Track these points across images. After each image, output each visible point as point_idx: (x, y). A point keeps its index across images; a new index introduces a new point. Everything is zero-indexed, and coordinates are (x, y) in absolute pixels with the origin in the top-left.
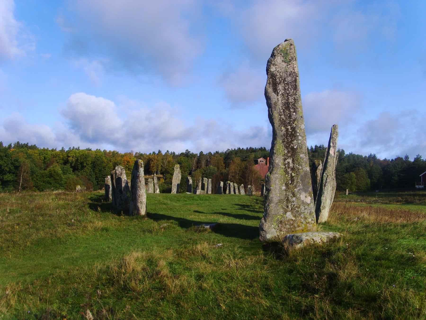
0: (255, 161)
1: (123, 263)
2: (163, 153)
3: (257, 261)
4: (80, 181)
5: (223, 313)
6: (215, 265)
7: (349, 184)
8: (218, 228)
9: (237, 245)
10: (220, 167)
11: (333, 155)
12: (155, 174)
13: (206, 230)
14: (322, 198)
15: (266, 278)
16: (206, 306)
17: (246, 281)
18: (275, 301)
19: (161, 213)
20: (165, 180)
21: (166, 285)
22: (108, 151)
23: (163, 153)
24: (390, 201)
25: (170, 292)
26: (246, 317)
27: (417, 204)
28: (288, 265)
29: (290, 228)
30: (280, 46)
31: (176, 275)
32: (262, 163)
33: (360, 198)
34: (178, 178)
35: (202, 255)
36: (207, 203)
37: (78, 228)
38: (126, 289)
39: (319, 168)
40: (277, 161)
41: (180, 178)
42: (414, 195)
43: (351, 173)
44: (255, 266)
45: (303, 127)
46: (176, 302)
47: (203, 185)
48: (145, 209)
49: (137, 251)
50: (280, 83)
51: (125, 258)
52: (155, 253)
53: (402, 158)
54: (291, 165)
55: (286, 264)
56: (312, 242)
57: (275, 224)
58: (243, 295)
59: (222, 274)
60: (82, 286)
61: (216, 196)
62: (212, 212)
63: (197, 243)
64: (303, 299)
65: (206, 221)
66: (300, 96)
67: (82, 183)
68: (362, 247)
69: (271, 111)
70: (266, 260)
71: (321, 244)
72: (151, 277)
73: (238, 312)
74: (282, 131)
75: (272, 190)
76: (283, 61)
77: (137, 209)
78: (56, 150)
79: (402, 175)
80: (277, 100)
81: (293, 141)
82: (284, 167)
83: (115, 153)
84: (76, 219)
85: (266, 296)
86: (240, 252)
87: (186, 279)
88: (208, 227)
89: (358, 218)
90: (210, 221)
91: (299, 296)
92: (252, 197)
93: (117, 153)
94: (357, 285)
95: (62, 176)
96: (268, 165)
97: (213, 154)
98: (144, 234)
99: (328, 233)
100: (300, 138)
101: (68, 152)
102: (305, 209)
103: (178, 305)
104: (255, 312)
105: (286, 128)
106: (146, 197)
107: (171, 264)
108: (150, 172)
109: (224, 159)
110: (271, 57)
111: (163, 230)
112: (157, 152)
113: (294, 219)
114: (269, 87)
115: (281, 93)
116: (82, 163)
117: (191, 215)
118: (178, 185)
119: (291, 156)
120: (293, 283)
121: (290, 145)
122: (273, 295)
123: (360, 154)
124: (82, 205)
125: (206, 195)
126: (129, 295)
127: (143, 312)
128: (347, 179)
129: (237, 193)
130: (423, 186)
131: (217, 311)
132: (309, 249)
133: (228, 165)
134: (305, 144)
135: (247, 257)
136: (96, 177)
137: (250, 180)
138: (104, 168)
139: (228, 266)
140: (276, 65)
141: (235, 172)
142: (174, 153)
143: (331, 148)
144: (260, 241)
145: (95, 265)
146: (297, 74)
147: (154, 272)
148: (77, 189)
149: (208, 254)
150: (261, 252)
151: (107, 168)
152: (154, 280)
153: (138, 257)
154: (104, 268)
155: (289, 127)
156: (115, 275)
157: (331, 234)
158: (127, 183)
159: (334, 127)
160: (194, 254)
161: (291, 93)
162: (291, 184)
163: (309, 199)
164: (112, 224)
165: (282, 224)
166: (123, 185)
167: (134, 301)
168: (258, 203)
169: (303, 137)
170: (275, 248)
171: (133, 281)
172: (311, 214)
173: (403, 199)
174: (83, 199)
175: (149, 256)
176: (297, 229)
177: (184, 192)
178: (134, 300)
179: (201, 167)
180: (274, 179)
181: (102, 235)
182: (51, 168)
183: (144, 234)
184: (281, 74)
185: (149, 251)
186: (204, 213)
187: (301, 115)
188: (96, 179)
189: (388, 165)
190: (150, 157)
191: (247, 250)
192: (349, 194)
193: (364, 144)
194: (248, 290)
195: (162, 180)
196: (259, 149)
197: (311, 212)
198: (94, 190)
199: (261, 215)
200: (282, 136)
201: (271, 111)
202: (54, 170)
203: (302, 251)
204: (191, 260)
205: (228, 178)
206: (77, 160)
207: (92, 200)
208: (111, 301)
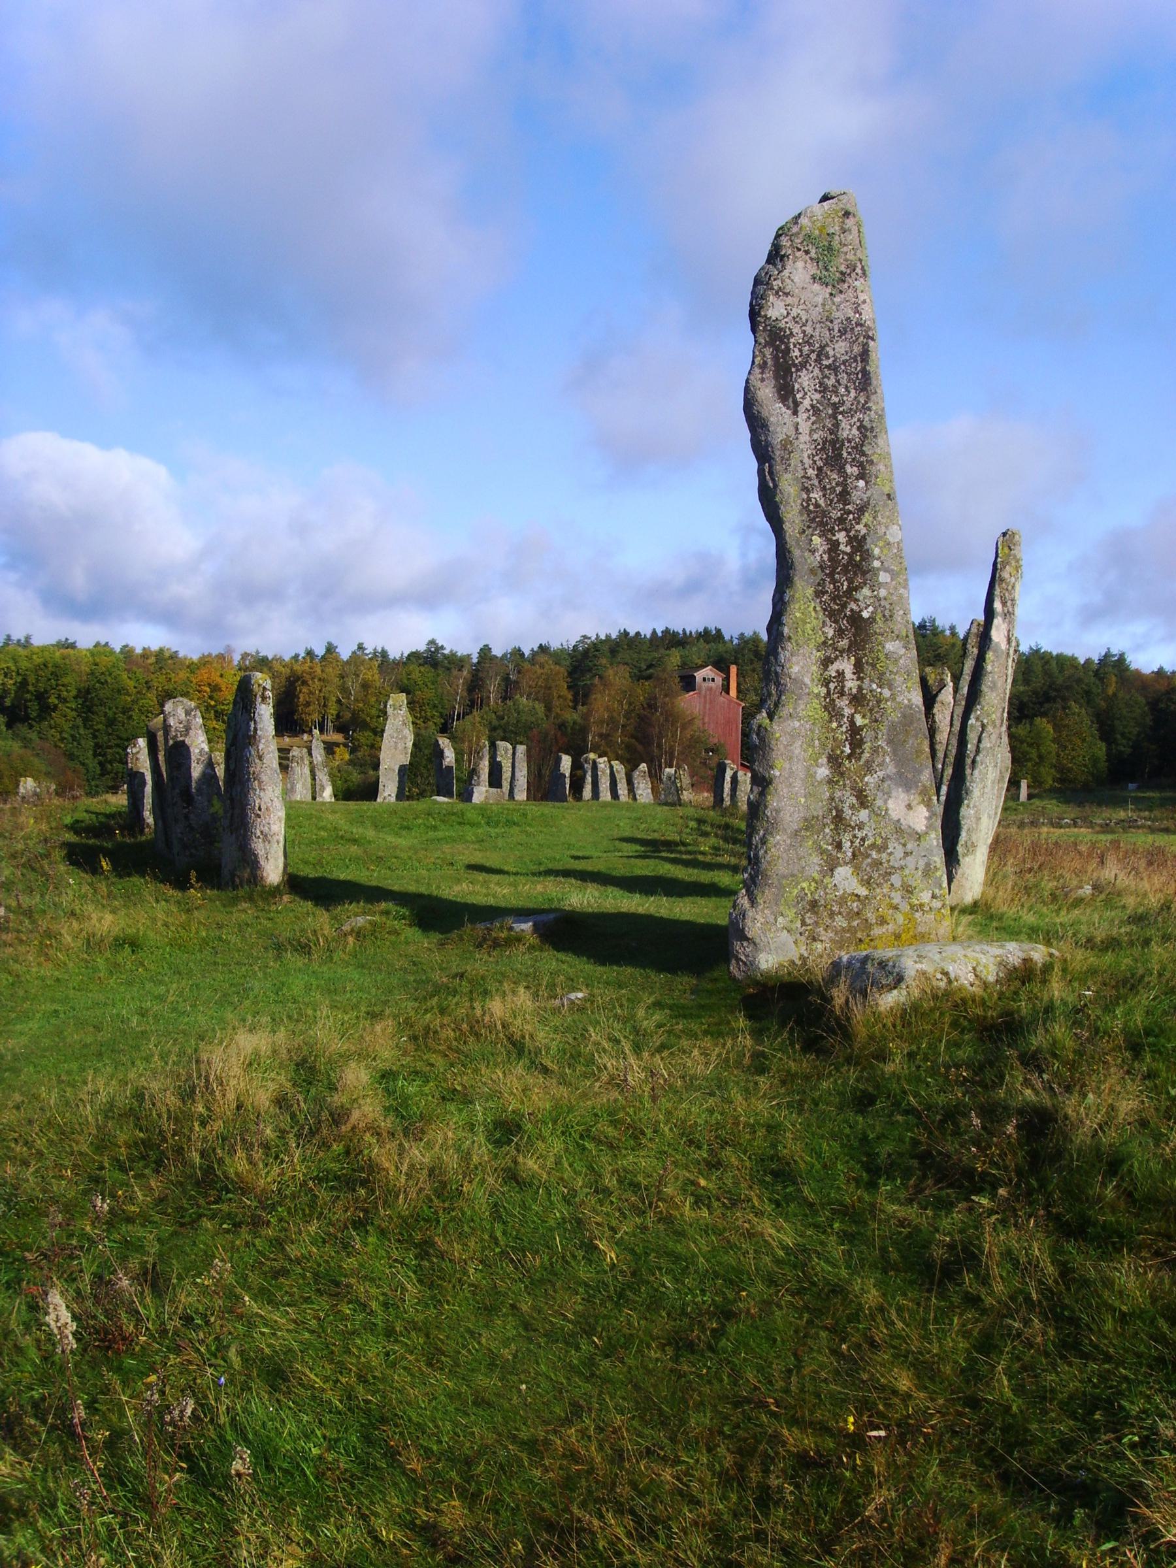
0: (682, 678)
1: (199, 1078)
2: (345, 653)
3: (727, 1060)
4: (36, 761)
5: (608, 1278)
6: (563, 1081)
7: (1030, 759)
8: (565, 932)
9: (643, 996)
10: (556, 702)
11: (1004, 646)
12: (316, 732)
13: (519, 940)
14: (963, 811)
15: (772, 1128)
16: (537, 1252)
17: (691, 1142)
18: (816, 1226)
19: (342, 877)
20: (353, 751)
21: (372, 1167)
22: (139, 651)
23: (345, 653)
25: (392, 1193)
26: (703, 1292)
28: (853, 1074)
29: (850, 929)
30: (804, 221)
31: (410, 1124)
33: (1070, 812)
34: (401, 746)
35: (510, 1038)
36: (510, 838)
37: (21, 941)
38: (210, 1182)
39: (940, 697)
40: (795, 669)
41: (410, 744)
43: (1038, 720)
44: (719, 1080)
45: (894, 534)
46: (418, 1240)
48: (281, 860)
49: (252, 1030)
50: (803, 365)
51: (204, 1057)
52: (326, 1034)
55: (844, 1069)
56: (942, 984)
57: (791, 913)
58: (683, 1203)
59: (596, 1115)
60: (37, 1171)
61: (548, 808)
62: (534, 868)
63: (486, 993)
64: (929, 1212)
65: (515, 902)
66: (881, 417)
67: (43, 768)
68: (1145, 998)
69: (771, 473)
70: (763, 1054)
71: (977, 990)
72: (312, 1133)
73: (669, 1271)
74: (813, 552)
75: (775, 781)
76: (814, 278)
77: (251, 862)
80: (792, 433)
81: (856, 589)
82: (824, 690)
84: (14, 904)
85: (778, 1204)
86: (659, 1026)
87: (451, 1141)
88: (527, 926)
89: (1094, 887)
90: (531, 905)
91: (910, 1201)
92: (681, 811)
93: (174, 656)
94: (1143, 1160)
96: (733, 692)
97: (527, 653)
98: (278, 957)
99: (1002, 946)
100: (883, 577)
102: (907, 854)
103: (424, 1249)
104: (739, 1272)
105: (829, 540)
107: (386, 1076)
108: (295, 722)
109: (570, 674)
110: (768, 262)
111: (351, 939)
112: (320, 651)
113: (863, 891)
114: (762, 380)
116: (41, 697)
117: (459, 881)
118: (402, 770)
119: (849, 650)
120: (885, 1150)
122: (805, 1199)
123: (1068, 652)
124: (40, 849)
125: (511, 805)
126: (225, 1207)
127: (281, 1280)
128: (1022, 742)
129: (624, 800)
131: (584, 1272)
132: (932, 1010)
134: (903, 602)
135: (685, 1043)
136: (97, 746)
137: (666, 747)
138: (126, 711)
139: (617, 1083)
140: (787, 294)
141: (612, 721)
142: (384, 654)
143: (997, 621)
144: (733, 979)
145: (90, 1087)
146: (869, 328)
147: (325, 1115)
148: (22, 790)
149: (531, 1036)
150: (742, 1022)
151: (135, 714)
152: (325, 1145)
153: (257, 1053)
154: (124, 1100)
155: (841, 537)
156: (168, 1126)
157: (1014, 952)
158: (210, 764)
160: (477, 1035)
161: (848, 404)
162: (849, 757)
163: (920, 817)
164: (154, 920)
165: (816, 913)
166: (196, 771)
167: (245, 1233)
168: (706, 834)
169: (894, 575)
170: (796, 1008)
171: (240, 1154)
172: (928, 871)
174: (44, 827)
175: (299, 1048)
177: (422, 795)
178: (244, 1230)
179: (484, 702)
180: (784, 740)
181: (116, 965)
183: (278, 957)
185: (301, 1026)
186: (507, 873)
187: (886, 490)
188: (95, 755)
190: (296, 667)
191: (685, 1017)
192: (1030, 797)
193: (1090, 616)
194: (703, 1183)
195: (343, 754)
196: (699, 635)
197: (928, 865)
198: (89, 794)
199: (724, 879)
200: (812, 571)
201: (771, 473)
203: (902, 1017)
204: (466, 1060)
205: (585, 740)
207: (77, 832)
208: (149, 1236)
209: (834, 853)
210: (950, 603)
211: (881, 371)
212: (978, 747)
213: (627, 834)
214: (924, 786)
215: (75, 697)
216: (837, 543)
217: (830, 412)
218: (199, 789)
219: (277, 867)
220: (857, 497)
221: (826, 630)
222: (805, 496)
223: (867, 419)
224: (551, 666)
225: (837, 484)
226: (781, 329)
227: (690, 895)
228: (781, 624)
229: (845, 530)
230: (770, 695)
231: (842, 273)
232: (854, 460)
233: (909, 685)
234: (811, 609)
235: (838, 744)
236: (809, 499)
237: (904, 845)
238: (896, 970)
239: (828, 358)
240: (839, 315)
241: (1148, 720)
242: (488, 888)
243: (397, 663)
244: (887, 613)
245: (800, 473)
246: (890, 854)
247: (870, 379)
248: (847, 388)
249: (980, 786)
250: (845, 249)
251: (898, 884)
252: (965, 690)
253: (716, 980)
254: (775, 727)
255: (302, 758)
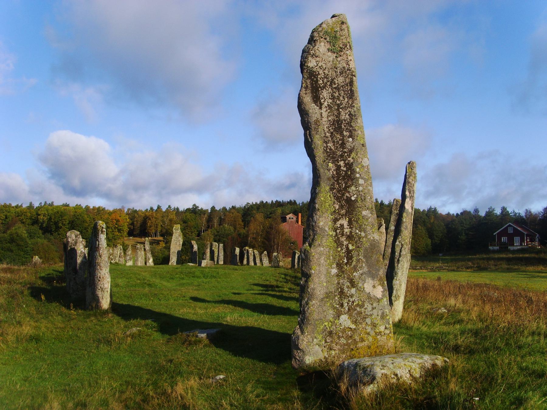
2: (164, 209)
4: (52, 247)
10: (238, 226)
11: (410, 210)
13: (200, 341)
22: (91, 207)
23: (164, 209)
24: (458, 268)
27: (492, 271)
29: (348, 344)
30: (324, 26)
32: (292, 220)
34: (178, 243)
40: (321, 224)
41: (181, 243)
42: (488, 259)
45: (365, 162)
47: (212, 252)
50: (324, 87)
53: (470, 212)
54: (346, 230)
56: (394, 381)
57: (320, 337)
62: (217, 299)
65: (205, 319)
66: (359, 110)
69: (310, 135)
74: (329, 170)
75: (312, 276)
76: (328, 50)
77: (96, 300)
78: (21, 206)
79: (470, 233)
80: (319, 117)
81: (349, 187)
82: (334, 233)
83: (101, 209)
90: (211, 320)
92: (278, 270)
93: (104, 209)
95: (28, 240)
96: (300, 223)
97: (228, 209)
99: (422, 358)
100: (361, 181)
101: (39, 208)
102: (373, 309)
105: (336, 165)
106: (109, 280)
109: (243, 216)
110: (308, 43)
111: (129, 339)
112: (155, 208)
113: (353, 326)
114: (306, 94)
115: (326, 104)
116: (56, 223)
117: (184, 306)
118: (178, 252)
119: (346, 215)
121: (343, 195)
129: (259, 262)
130: (498, 248)
133: (248, 224)
137: (276, 242)
140: (317, 57)
142: (178, 209)
143: (407, 200)
146: (353, 72)
150: (296, 393)
155: (342, 163)
157: (427, 360)
159: (411, 165)
161: (344, 105)
162: (346, 264)
163: (379, 291)
168: (287, 282)
169: (366, 180)
173: (474, 264)
176: (360, 345)
179: (213, 226)
181: (27, 350)
182: (13, 230)
184: (326, 72)
187: (362, 142)
189: (453, 221)
190: (147, 214)
196: (288, 202)
197: (383, 313)
200: (329, 179)
201: (310, 135)
202: (16, 233)
203: (376, 400)
206: (50, 218)
209: (340, 309)
210: (386, 191)
211: (358, 90)
212: (400, 254)
213: (256, 282)
214: (381, 277)
215: (68, 224)
216: (340, 166)
217: (336, 108)
218: (80, 267)
219: (107, 302)
220: (349, 145)
221: (335, 205)
222: (325, 145)
223: (353, 111)
224: (236, 213)
225: (340, 140)
226: (314, 72)
227: (278, 314)
228: (315, 203)
229: (344, 160)
230: (310, 235)
231: (341, 48)
232: (347, 129)
233: (373, 230)
234: (328, 196)
235: (341, 258)
236: (327, 146)
237: (372, 304)
238: (372, 373)
239: (335, 84)
240: (340, 66)
241: (445, 231)
242: (195, 310)
243: (182, 212)
244: (363, 198)
245: (323, 135)
246: (366, 309)
247: (354, 93)
248: (343, 97)
249: (401, 271)
250: (342, 38)
251: (369, 323)
252: (392, 228)
253: (285, 368)
254: (312, 250)
255: (141, 248)
